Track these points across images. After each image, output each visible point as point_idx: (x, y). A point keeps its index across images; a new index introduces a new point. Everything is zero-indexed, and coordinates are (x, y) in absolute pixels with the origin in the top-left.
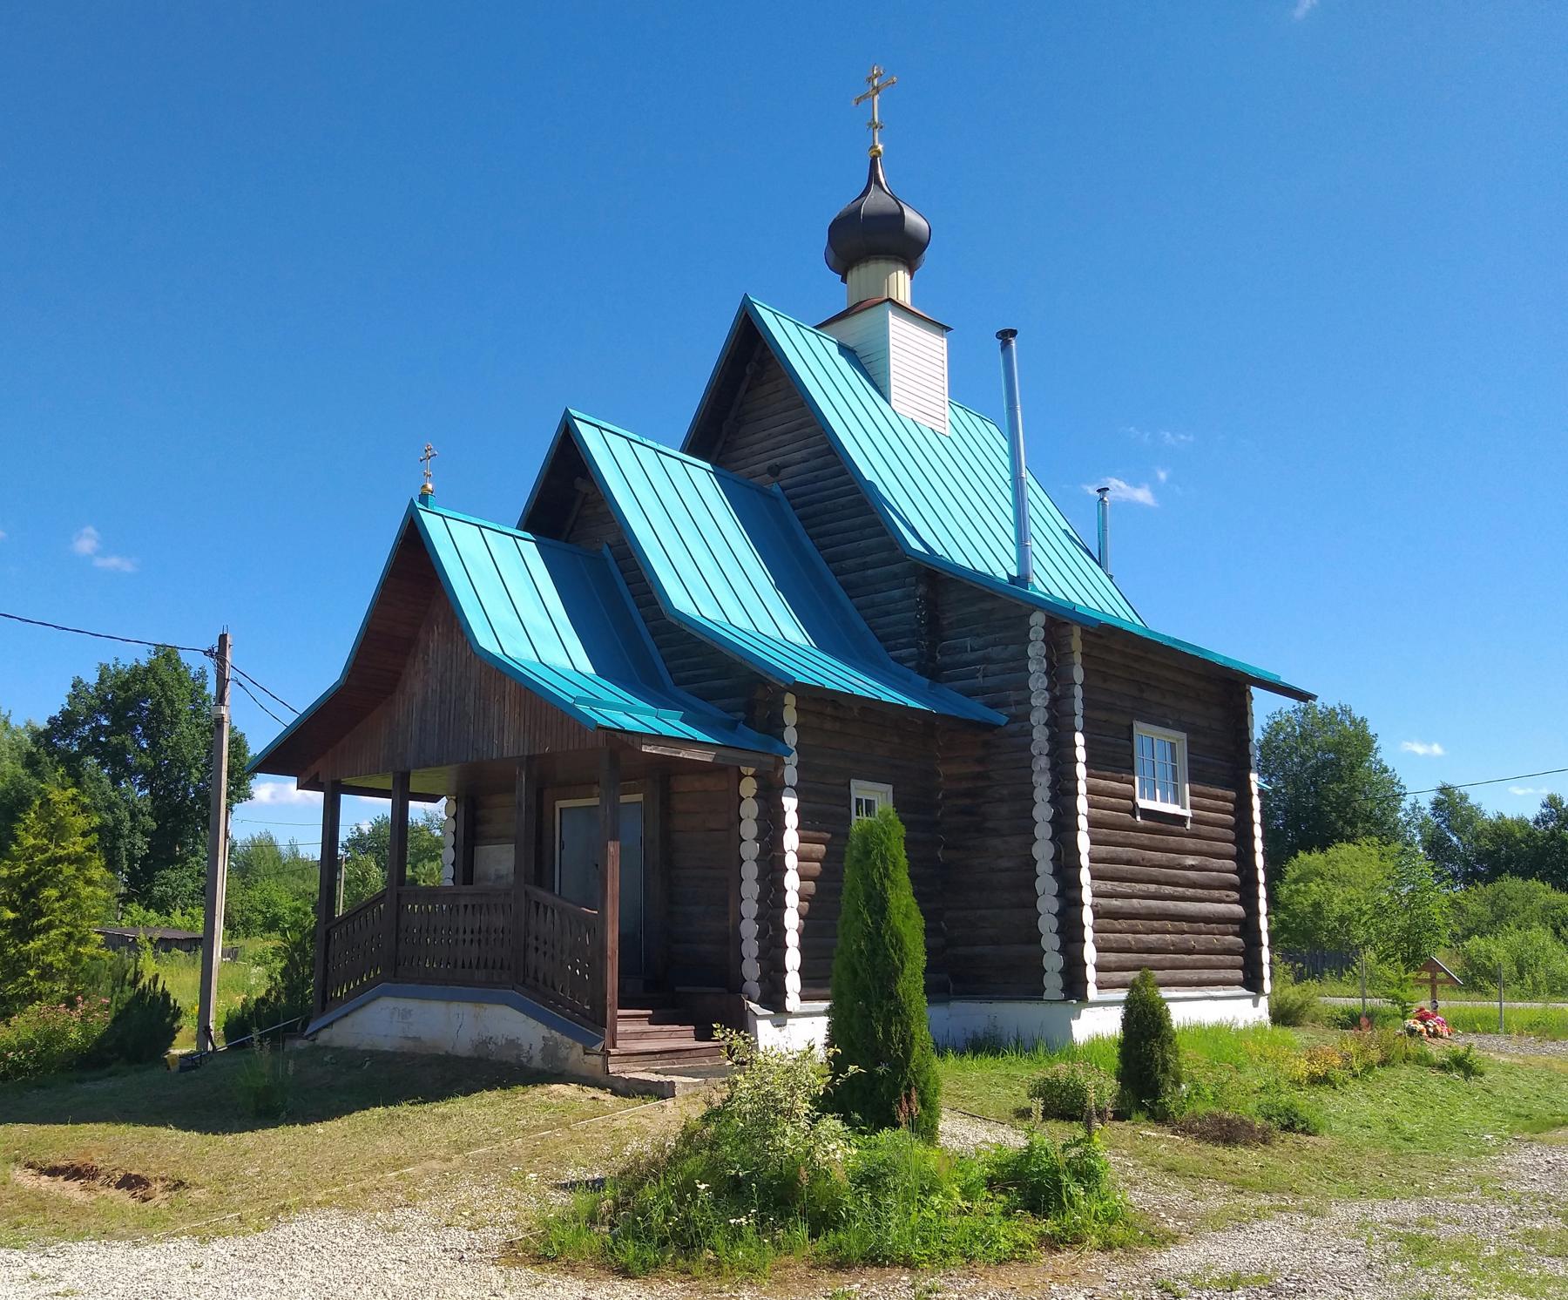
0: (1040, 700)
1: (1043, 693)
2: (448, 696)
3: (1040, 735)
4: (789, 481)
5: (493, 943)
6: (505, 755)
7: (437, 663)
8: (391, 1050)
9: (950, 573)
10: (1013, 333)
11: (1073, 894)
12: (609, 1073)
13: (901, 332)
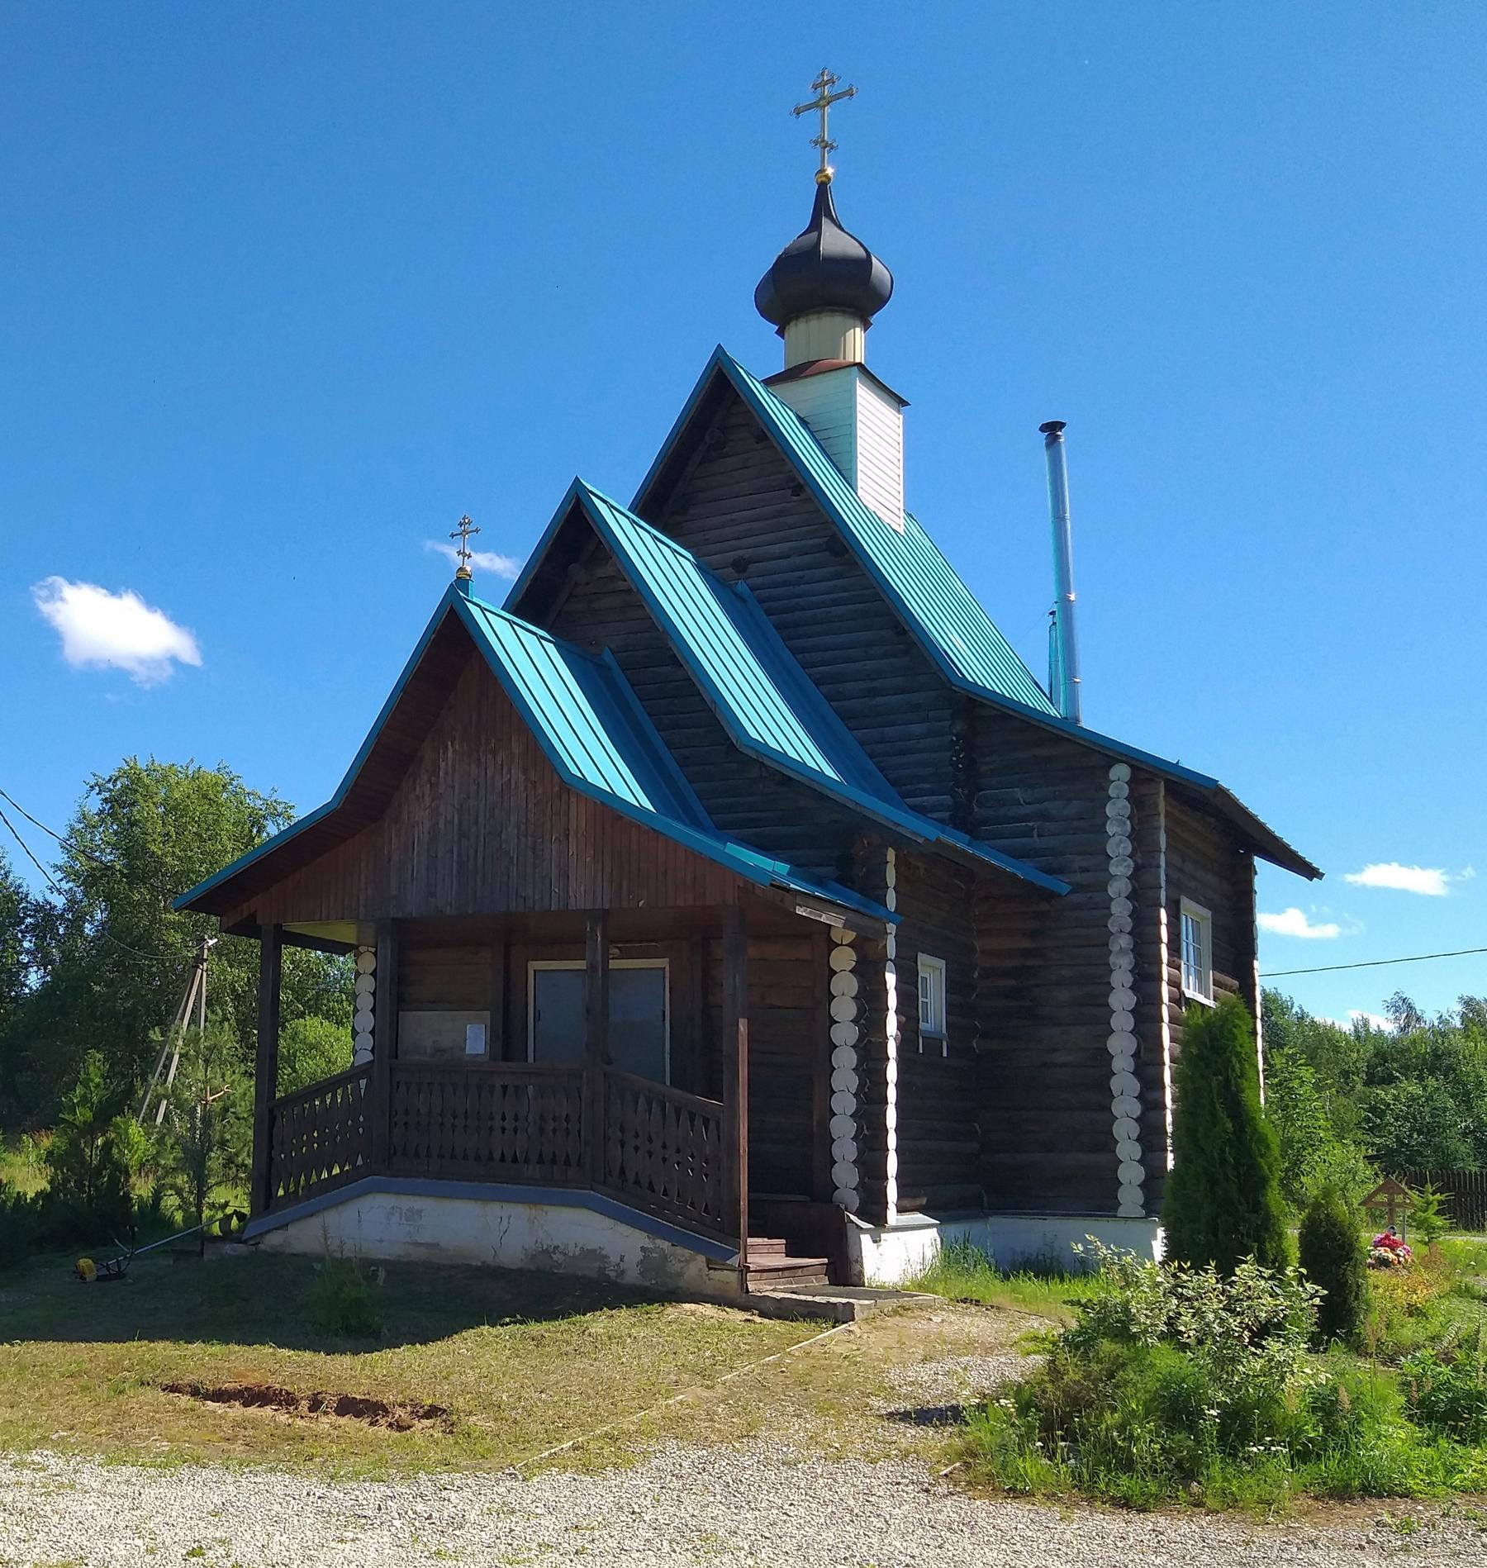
0: (1120, 869)
1: (1126, 860)
2: (473, 829)
3: (1121, 910)
4: (759, 580)
5: (551, 1133)
6: (572, 905)
7: (453, 787)
8: (392, 1259)
9: (1015, 711)
10: (1061, 425)
11: (1154, 1095)
12: (748, 1291)
13: (870, 408)
